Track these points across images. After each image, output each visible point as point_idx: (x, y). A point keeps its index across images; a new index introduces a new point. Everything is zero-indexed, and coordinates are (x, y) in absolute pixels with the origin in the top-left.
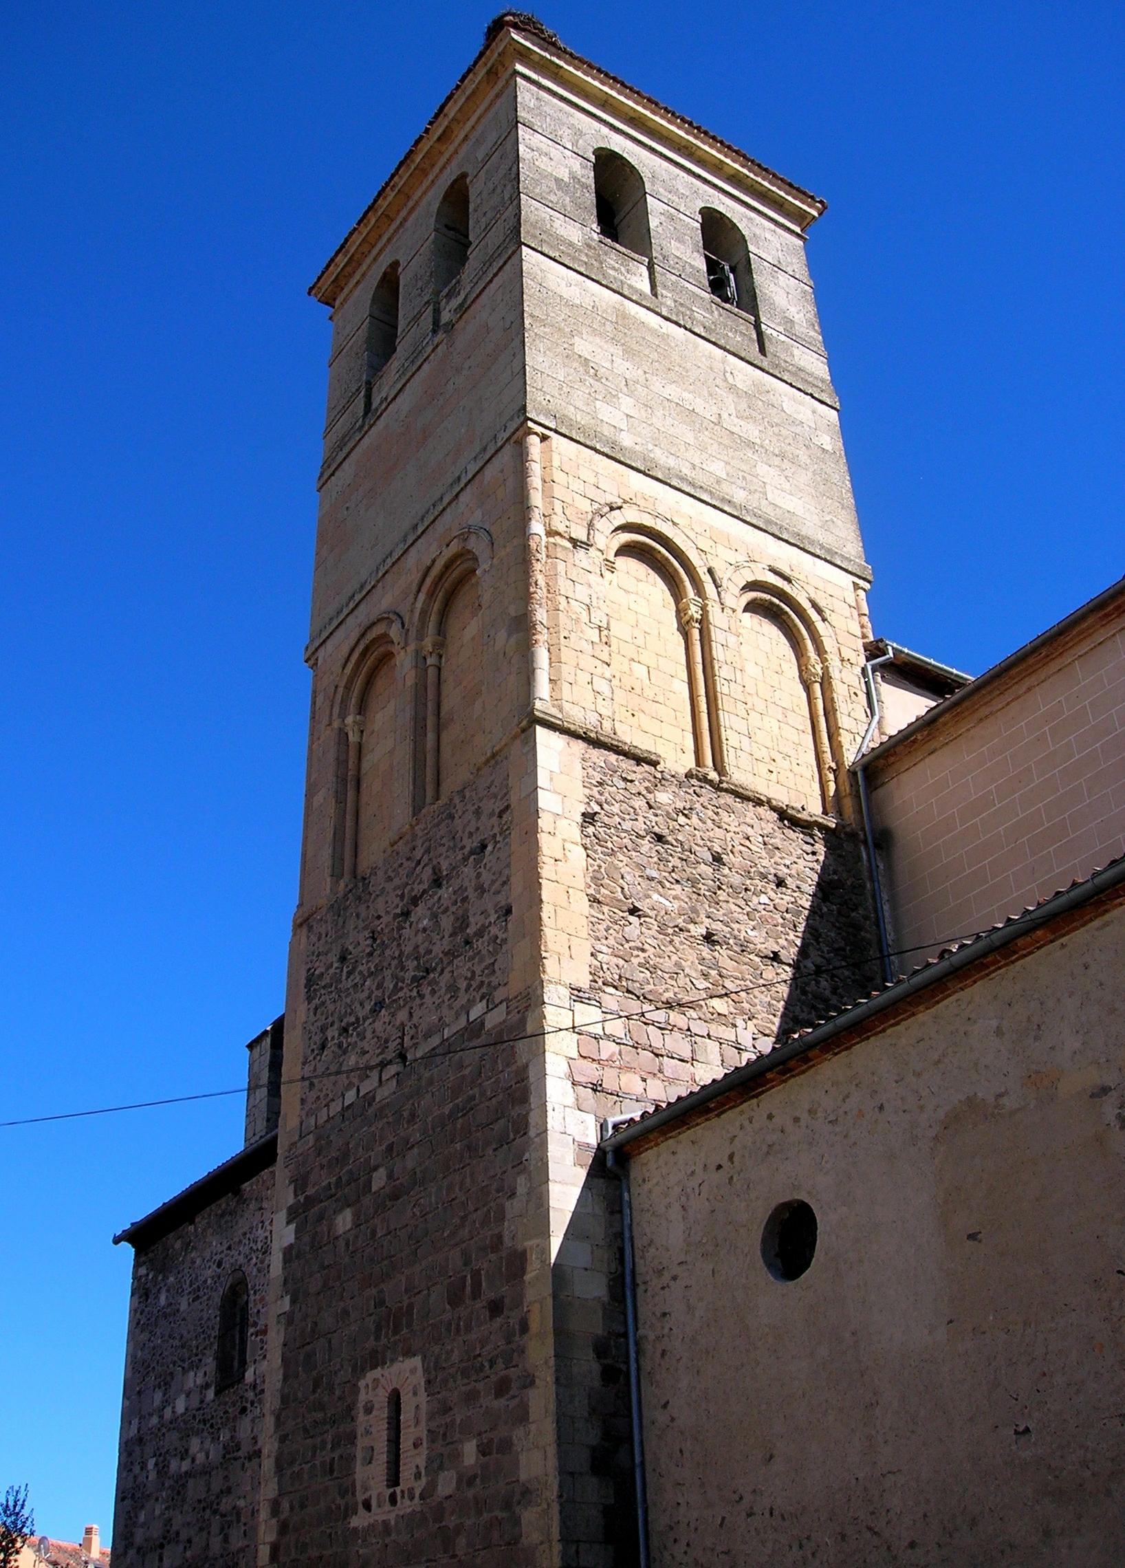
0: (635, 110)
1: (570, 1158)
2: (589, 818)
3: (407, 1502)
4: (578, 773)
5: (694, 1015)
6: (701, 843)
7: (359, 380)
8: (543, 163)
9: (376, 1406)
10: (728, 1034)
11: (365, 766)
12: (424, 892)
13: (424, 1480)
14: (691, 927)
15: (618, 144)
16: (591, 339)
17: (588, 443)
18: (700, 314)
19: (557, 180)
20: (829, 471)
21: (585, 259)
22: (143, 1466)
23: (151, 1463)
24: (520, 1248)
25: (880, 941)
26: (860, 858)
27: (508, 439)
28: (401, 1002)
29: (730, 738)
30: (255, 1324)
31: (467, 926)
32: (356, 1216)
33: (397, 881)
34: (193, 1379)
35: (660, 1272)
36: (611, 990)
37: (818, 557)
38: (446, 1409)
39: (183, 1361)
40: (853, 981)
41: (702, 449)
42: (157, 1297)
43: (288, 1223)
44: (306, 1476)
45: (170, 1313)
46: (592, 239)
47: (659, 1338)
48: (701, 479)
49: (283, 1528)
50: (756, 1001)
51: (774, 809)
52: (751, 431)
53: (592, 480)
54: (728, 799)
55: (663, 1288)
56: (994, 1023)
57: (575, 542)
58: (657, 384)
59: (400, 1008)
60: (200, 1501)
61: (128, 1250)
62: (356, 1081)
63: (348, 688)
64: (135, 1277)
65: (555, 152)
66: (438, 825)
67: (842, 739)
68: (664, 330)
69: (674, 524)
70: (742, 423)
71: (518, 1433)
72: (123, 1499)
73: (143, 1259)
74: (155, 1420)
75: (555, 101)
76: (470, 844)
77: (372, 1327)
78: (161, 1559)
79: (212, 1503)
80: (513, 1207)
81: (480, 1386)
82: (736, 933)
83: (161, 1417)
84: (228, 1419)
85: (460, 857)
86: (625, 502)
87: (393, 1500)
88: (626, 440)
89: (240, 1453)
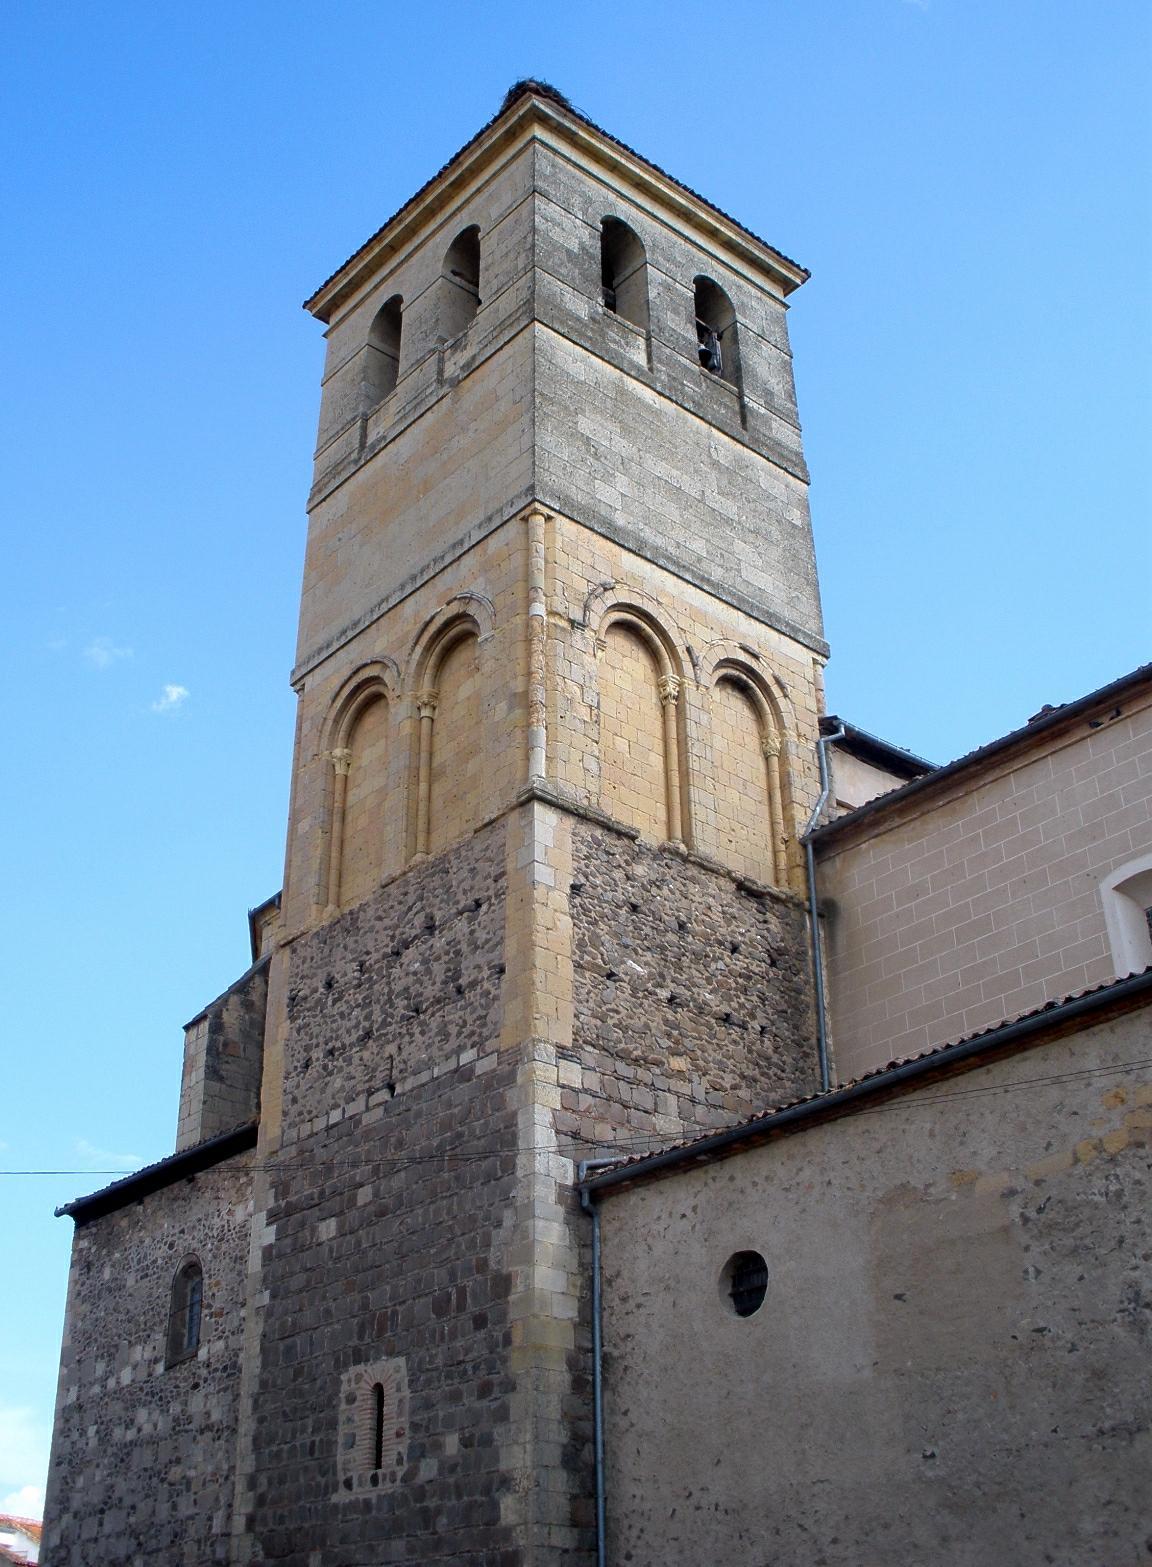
0: (641, 178)
1: (552, 1198)
2: (576, 889)
3: (388, 1484)
4: (570, 847)
5: (657, 1071)
6: (670, 912)
7: (356, 409)
8: (556, 235)
9: (359, 1398)
10: (686, 1089)
11: (351, 799)
12: (416, 937)
13: (406, 1466)
14: (658, 991)
15: (624, 212)
16: (592, 417)
17: (588, 524)
18: (690, 387)
19: (568, 252)
20: (797, 546)
21: (590, 334)
22: (83, 1432)
23: (92, 1430)
24: (504, 1271)
25: (817, 1006)
26: (803, 926)
27: (515, 515)
28: (390, 1037)
29: (699, 813)
30: (209, 1306)
31: (459, 977)
32: (340, 1227)
33: (387, 922)
34: (139, 1353)
35: (624, 1300)
36: (589, 1048)
37: (784, 634)
38: (428, 1405)
39: (130, 1334)
40: (793, 1041)
41: (686, 526)
42: (100, 1271)
43: (268, 1225)
44: (285, 1455)
45: (116, 1288)
46: (597, 312)
47: (622, 1357)
48: (686, 560)
49: (261, 1501)
50: (710, 1059)
51: (734, 880)
52: (730, 508)
53: (589, 561)
54: (693, 871)
55: (627, 1314)
56: (928, 1126)
57: (572, 622)
58: (649, 461)
59: (389, 1042)
60: (145, 1470)
61: (69, 1222)
62: (342, 1103)
63: (336, 721)
64: (76, 1250)
65: (567, 221)
66: (433, 875)
67: (795, 812)
68: (657, 406)
69: (659, 603)
70: (723, 500)
71: (498, 1431)
72: (59, 1464)
73: (83, 1232)
74: (97, 1389)
75: (569, 167)
76: (465, 901)
77: (356, 1329)
78: (101, 1524)
79: (159, 1473)
80: (499, 1236)
81: (463, 1387)
82: (696, 996)
83: (104, 1387)
84: (179, 1394)
85: (454, 911)
86: (617, 582)
87: (375, 1480)
88: (620, 520)
89: (190, 1427)
